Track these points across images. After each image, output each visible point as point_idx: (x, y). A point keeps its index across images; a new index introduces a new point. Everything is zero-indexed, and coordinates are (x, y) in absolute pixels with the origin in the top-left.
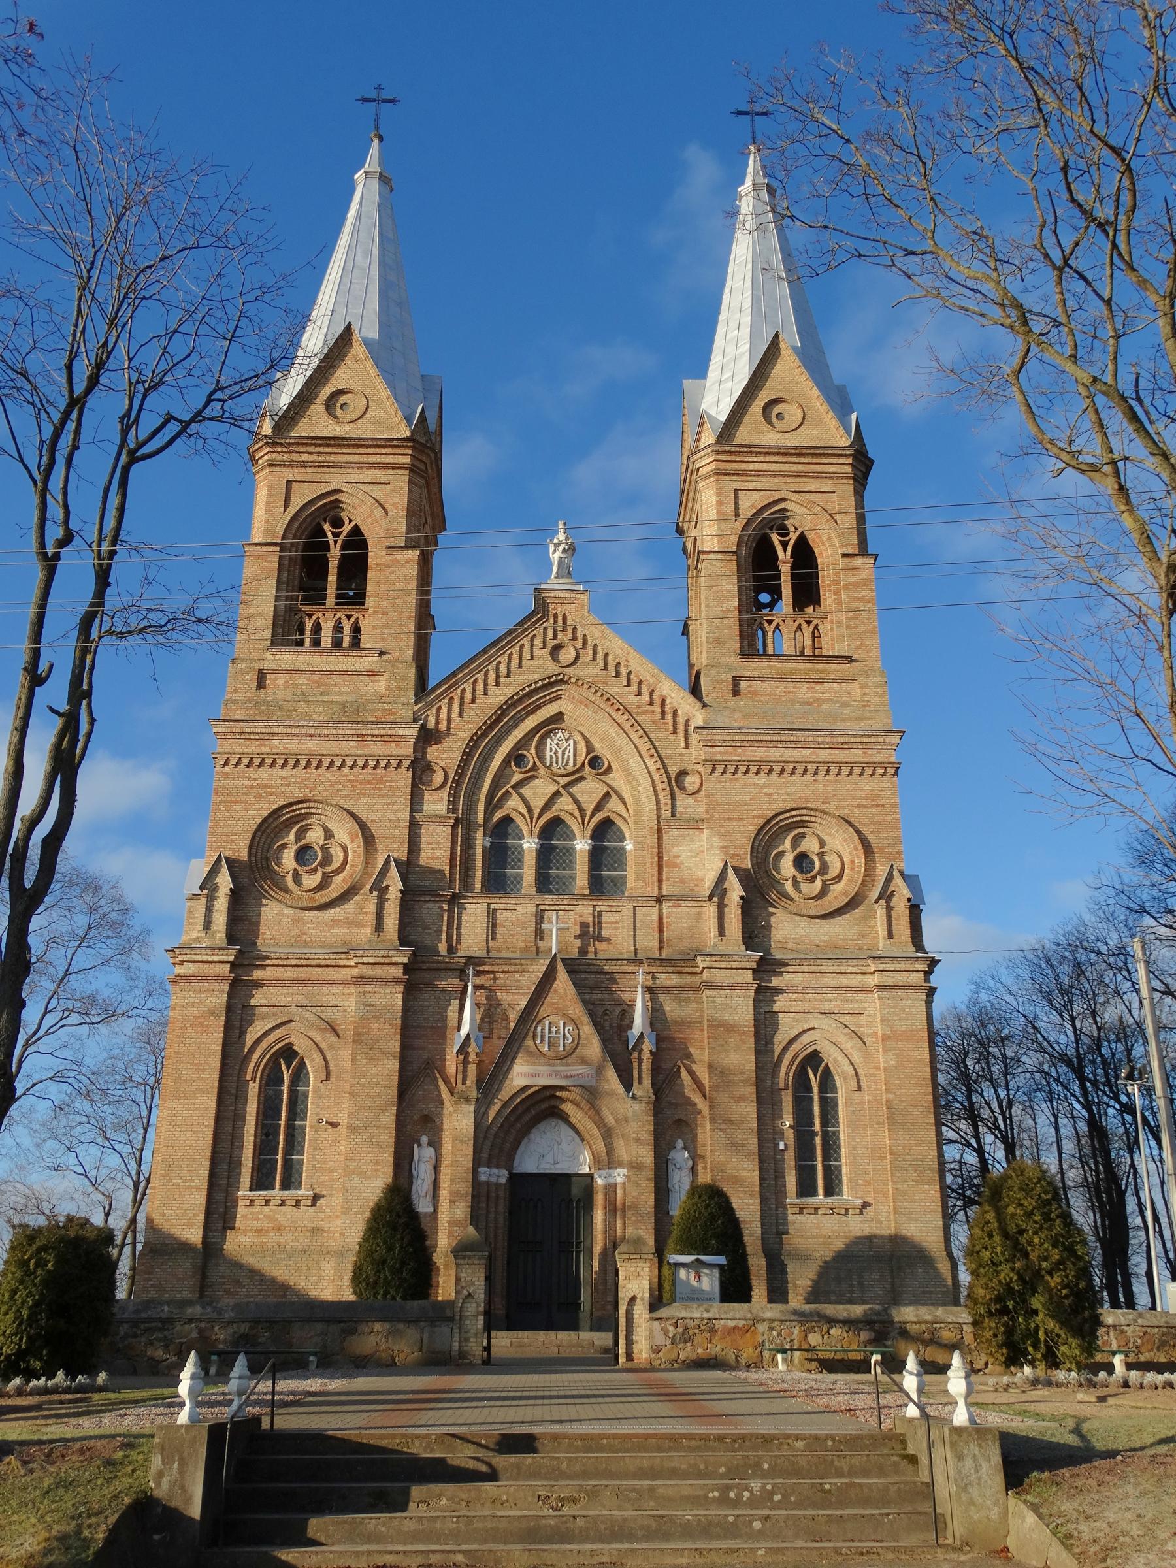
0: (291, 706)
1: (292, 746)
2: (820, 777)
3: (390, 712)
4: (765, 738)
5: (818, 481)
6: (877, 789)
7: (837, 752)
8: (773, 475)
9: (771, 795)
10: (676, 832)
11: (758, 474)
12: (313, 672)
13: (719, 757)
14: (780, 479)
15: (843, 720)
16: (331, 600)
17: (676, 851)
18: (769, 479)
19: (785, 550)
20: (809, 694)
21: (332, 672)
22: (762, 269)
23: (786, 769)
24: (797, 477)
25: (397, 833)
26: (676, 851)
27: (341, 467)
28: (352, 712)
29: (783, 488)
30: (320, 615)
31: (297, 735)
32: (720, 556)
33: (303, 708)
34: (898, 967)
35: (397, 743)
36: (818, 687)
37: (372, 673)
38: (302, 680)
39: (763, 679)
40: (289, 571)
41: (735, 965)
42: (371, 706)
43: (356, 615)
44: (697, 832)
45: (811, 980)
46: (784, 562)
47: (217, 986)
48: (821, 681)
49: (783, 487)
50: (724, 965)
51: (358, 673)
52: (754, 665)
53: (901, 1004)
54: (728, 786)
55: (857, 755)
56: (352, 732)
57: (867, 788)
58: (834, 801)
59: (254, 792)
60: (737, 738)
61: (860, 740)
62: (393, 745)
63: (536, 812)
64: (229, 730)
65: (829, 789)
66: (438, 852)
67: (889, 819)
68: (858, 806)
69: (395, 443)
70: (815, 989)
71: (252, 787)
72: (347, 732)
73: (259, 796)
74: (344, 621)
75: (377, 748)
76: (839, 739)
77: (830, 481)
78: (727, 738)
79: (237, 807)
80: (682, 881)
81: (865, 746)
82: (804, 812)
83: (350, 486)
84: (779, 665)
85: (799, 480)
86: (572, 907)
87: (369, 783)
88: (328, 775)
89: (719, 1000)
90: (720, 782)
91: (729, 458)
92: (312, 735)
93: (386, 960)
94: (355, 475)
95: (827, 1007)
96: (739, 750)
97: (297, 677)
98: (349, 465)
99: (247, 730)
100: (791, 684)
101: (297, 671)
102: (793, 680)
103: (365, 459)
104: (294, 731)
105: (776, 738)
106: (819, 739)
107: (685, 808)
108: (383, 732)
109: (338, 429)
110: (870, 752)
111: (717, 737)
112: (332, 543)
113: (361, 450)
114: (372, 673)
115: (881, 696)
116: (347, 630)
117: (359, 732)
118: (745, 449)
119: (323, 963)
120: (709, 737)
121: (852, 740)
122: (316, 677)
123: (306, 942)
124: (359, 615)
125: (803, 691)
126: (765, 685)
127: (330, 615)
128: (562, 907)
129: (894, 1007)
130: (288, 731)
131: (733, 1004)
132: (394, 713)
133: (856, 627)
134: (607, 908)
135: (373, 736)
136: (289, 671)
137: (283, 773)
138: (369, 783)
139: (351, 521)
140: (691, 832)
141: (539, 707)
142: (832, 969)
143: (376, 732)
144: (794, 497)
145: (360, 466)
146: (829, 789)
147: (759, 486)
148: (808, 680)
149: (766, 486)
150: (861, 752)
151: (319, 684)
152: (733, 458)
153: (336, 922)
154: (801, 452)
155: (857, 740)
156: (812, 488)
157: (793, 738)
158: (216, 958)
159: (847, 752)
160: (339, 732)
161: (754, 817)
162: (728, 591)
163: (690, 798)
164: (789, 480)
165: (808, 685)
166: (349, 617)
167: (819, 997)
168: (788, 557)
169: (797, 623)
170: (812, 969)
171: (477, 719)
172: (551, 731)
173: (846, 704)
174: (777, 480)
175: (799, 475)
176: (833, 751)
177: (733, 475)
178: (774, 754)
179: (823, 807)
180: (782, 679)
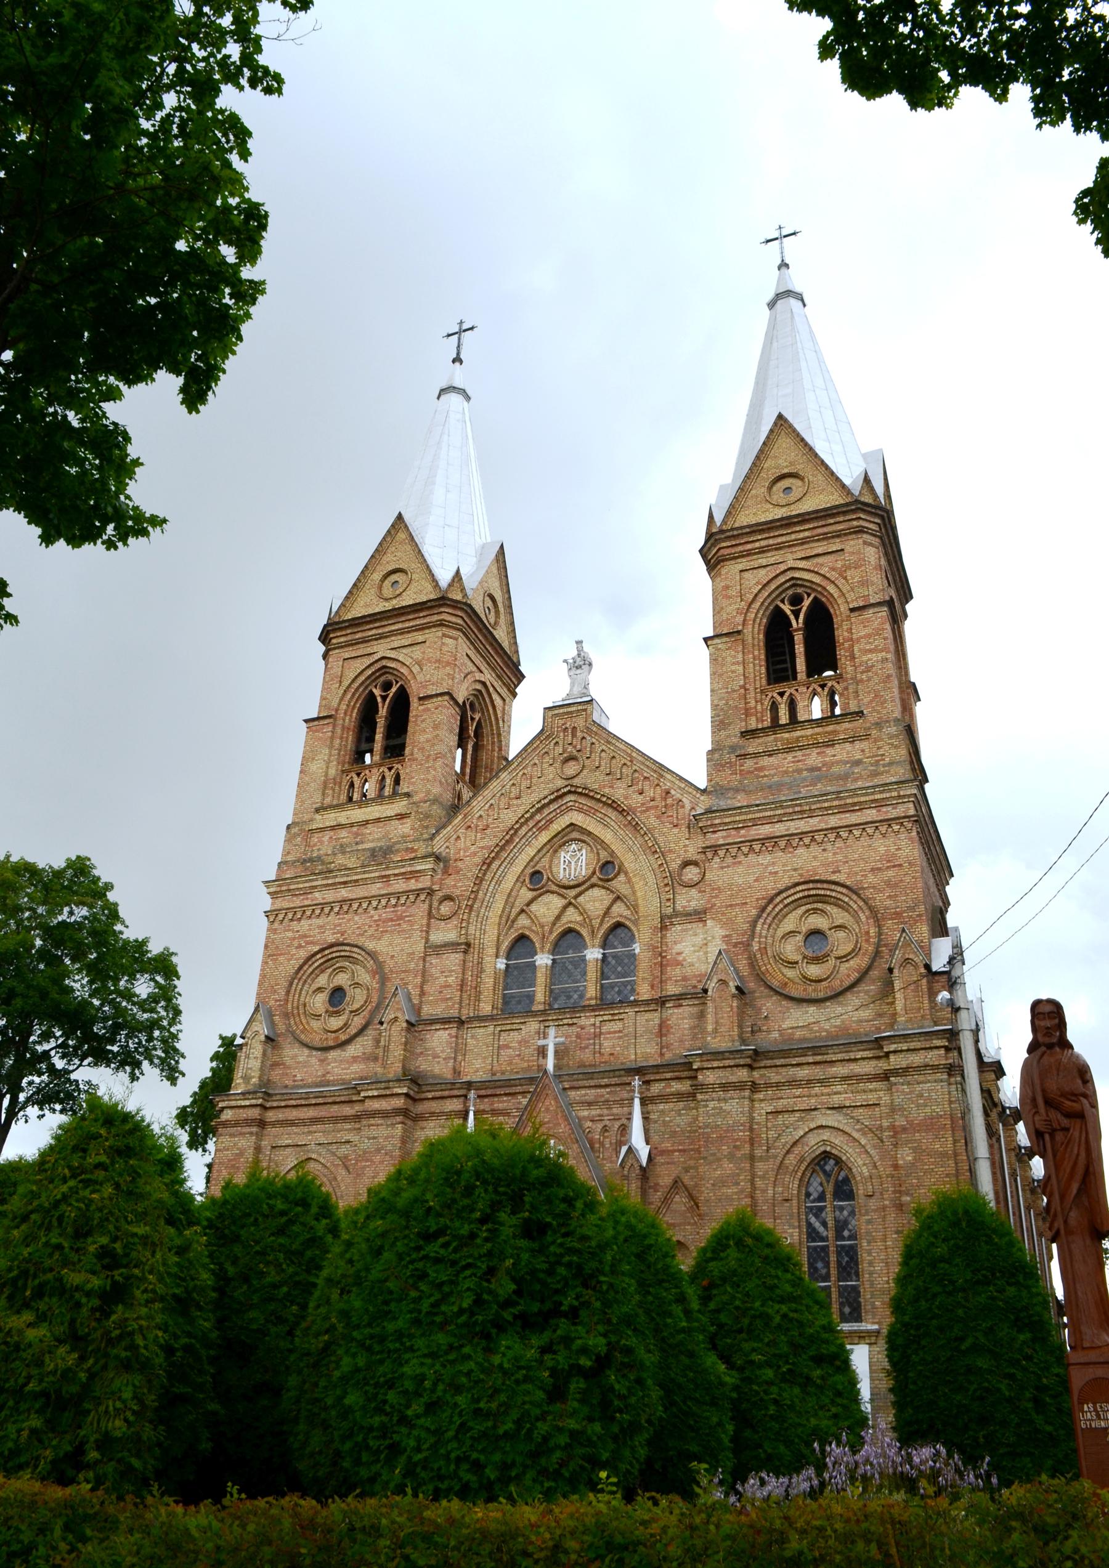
0: (330, 859)
1: (330, 896)
3: (412, 850)
6: (893, 849)
8: (778, 548)
9: (776, 873)
10: (679, 928)
11: (762, 551)
12: (352, 825)
13: (721, 842)
14: (787, 550)
15: (856, 780)
16: (802, 674)
17: (678, 948)
18: (773, 553)
19: (797, 618)
20: (820, 759)
21: (367, 822)
23: (791, 841)
24: (802, 544)
25: (412, 965)
26: (678, 948)
27: (386, 637)
28: (380, 855)
31: (334, 884)
32: (725, 639)
33: (340, 860)
34: (912, 1045)
35: (417, 878)
36: (829, 751)
37: (401, 817)
38: (343, 833)
40: (341, 738)
41: (727, 1063)
42: (397, 847)
43: (396, 766)
44: (701, 925)
45: (817, 1072)
46: (797, 630)
47: (247, 1129)
48: (830, 744)
49: (790, 556)
50: (715, 1064)
51: (389, 819)
52: (760, 740)
53: (918, 1088)
54: (730, 870)
55: (871, 814)
56: (377, 874)
57: (882, 849)
58: (845, 869)
59: (296, 943)
61: (871, 797)
62: (413, 881)
63: (596, 923)
64: (278, 889)
65: (839, 857)
66: (451, 980)
67: (908, 879)
68: (872, 870)
70: (820, 1081)
71: (294, 939)
72: (373, 875)
73: (300, 946)
74: (387, 773)
75: (400, 885)
76: (849, 801)
78: (727, 820)
79: (281, 959)
80: (685, 979)
81: (879, 804)
84: (786, 735)
85: (805, 546)
86: (575, 1020)
87: (392, 920)
88: (356, 918)
89: (711, 1104)
90: (722, 868)
92: (345, 883)
93: (388, 1092)
94: (397, 641)
95: (836, 1100)
96: (743, 832)
97: (339, 831)
98: (392, 633)
99: (292, 887)
100: (799, 753)
101: (340, 826)
102: (801, 748)
103: (407, 625)
104: (330, 881)
106: (826, 805)
107: (689, 901)
108: (403, 870)
109: (387, 604)
110: (884, 809)
111: (717, 821)
112: (792, 617)
113: (403, 619)
114: (401, 817)
115: (896, 747)
116: (389, 781)
117: (383, 873)
118: (748, 530)
119: (338, 1099)
121: (863, 799)
122: (355, 829)
123: (328, 1081)
124: (399, 766)
125: (814, 758)
126: (771, 759)
128: (565, 1021)
129: (911, 1092)
130: (325, 882)
131: (726, 1107)
132: (416, 851)
134: (610, 1017)
135: (395, 875)
136: (332, 828)
137: (320, 922)
138: (392, 920)
139: (397, 682)
140: (694, 925)
141: (551, 821)
142: (840, 1056)
143: (396, 871)
145: (402, 632)
146: (839, 857)
147: (764, 562)
148: (816, 745)
149: (772, 560)
151: (357, 834)
153: (355, 1059)
154: (804, 518)
155: (867, 798)
156: (820, 551)
157: (797, 809)
158: (247, 1103)
160: (367, 876)
161: (758, 899)
162: (733, 672)
165: (819, 750)
166: (781, 694)
167: (826, 1090)
168: (801, 625)
169: (811, 689)
170: (819, 1058)
171: (491, 843)
172: (584, 841)
173: (858, 763)
175: (804, 542)
176: (843, 816)
178: (779, 829)
179: (834, 878)
180: (789, 750)
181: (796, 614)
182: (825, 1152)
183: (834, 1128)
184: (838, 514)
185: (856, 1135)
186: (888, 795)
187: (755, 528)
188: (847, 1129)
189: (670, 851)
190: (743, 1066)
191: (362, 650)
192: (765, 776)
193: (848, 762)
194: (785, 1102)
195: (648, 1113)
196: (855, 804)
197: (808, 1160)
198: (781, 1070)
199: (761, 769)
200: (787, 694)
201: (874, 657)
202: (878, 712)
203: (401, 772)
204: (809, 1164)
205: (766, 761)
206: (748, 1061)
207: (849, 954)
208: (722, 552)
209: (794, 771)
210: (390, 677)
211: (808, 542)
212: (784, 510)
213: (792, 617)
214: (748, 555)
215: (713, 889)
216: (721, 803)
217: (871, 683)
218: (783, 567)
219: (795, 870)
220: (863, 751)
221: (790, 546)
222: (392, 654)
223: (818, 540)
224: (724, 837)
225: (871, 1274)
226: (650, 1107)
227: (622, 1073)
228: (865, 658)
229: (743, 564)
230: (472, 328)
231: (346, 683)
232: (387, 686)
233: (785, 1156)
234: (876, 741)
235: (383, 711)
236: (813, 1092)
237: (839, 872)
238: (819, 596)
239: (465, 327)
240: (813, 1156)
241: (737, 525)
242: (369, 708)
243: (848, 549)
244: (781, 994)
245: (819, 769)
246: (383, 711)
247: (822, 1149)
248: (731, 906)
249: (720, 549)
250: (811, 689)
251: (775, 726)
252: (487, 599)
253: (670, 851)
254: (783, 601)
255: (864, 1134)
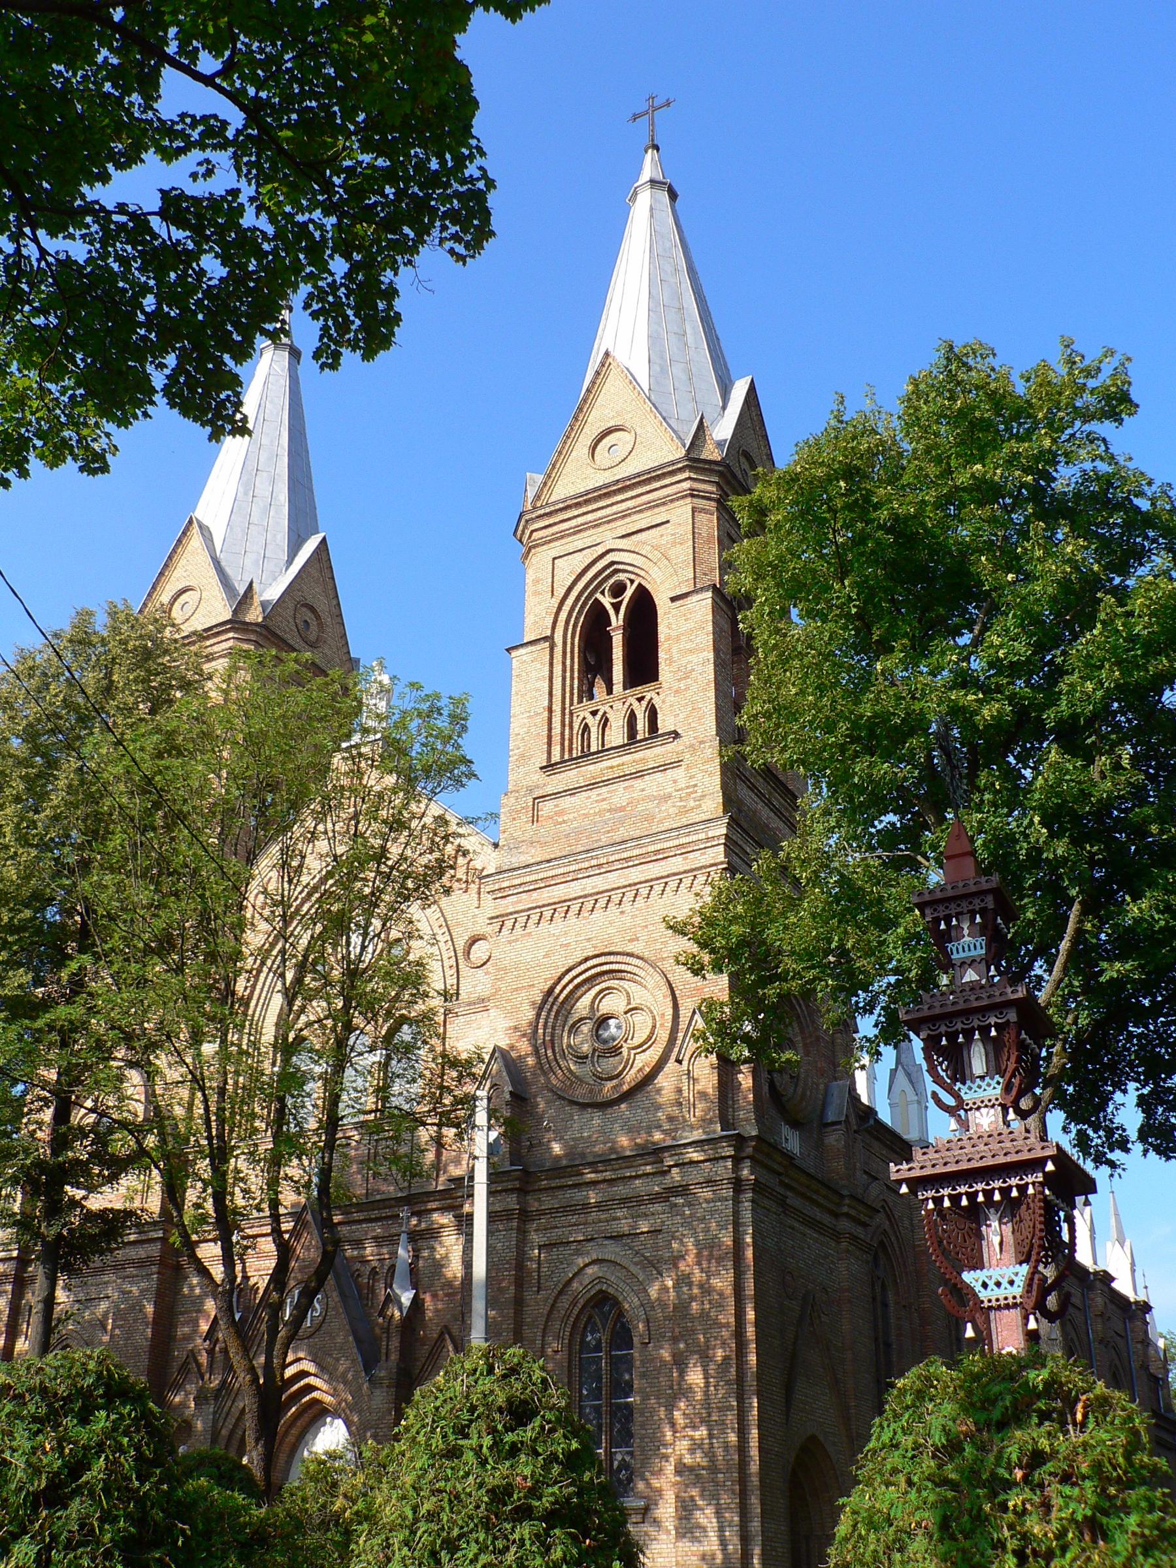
2: (626, 906)
4: (561, 871)
5: (649, 513)
7: (651, 865)
9: (568, 945)
22: (656, 256)
29: (607, 537)
30: (606, 708)
39: (572, 792)
48: (639, 775)
58: (643, 935)
60: (528, 879)
61: (676, 842)
69: (215, 630)
76: (651, 848)
77: (662, 509)
82: (611, 958)
83: (625, 541)
90: (510, 942)
91: (547, 523)
100: (604, 789)
105: (572, 868)
110: (691, 855)
112: (611, 612)
118: (561, 505)
120: (497, 887)
124: (653, 694)
126: (573, 799)
127: (618, 705)
133: (687, 689)
139: (632, 581)
144: (621, 544)
146: (638, 921)
147: (580, 545)
150: (679, 858)
152: (551, 521)
155: (670, 844)
157: (594, 862)
159: (662, 863)
163: (480, 971)
164: (613, 525)
167: (603, 1216)
168: (621, 622)
173: (667, 797)
174: (600, 529)
177: (550, 541)
181: (617, 607)
182: (601, 1291)
183: (610, 1261)
184: (664, 475)
185: (634, 1269)
186: (695, 838)
187: (570, 502)
188: (624, 1262)
189: (458, 924)
190: (512, 1190)
191: (579, 542)
192: (564, 822)
193: (655, 798)
194: (559, 1231)
195: (419, 1250)
196: (657, 852)
197: (582, 1302)
198: (559, 1193)
199: (561, 813)
200: (600, 713)
201: (693, 658)
202: (694, 729)
203: (657, 702)
204: (584, 1307)
205: (566, 802)
206: (517, 1184)
207: (644, 1043)
208: (536, 535)
209: (595, 814)
210: (622, 577)
211: (630, 515)
212: (607, 473)
213: (611, 612)
214: (562, 537)
215: (499, 970)
216: (513, 860)
217: (688, 694)
218: (600, 550)
219: (589, 940)
220: (675, 782)
221: (609, 522)
222: (621, 544)
223: (640, 511)
224: (513, 903)
225: (642, 1438)
226: (420, 1243)
227: (393, 1202)
228: (684, 661)
229: (557, 548)
230: (635, 117)
231: (559, 593)
232: (618, 589)
233: (557, 1298)
234: (688, 768)
235: (617, 621)
236: (590, 1219)
237: (637, 939)
238: (644, 583)
239: (657, 103)
240: (588, 1296)
241: (552, 499)
242: (596, 620)
243: (674, 519)
244: (564, 1099)
245: (622, 809)
246: (617, 621)
247: (597, 1288)
248: (516, 989)
249: (532, 532)
250: (627, 704)
251: (586, 755)
252: (743, 460)
253: (458, 924)
254: (603, 593)
255: (644, 1268)
